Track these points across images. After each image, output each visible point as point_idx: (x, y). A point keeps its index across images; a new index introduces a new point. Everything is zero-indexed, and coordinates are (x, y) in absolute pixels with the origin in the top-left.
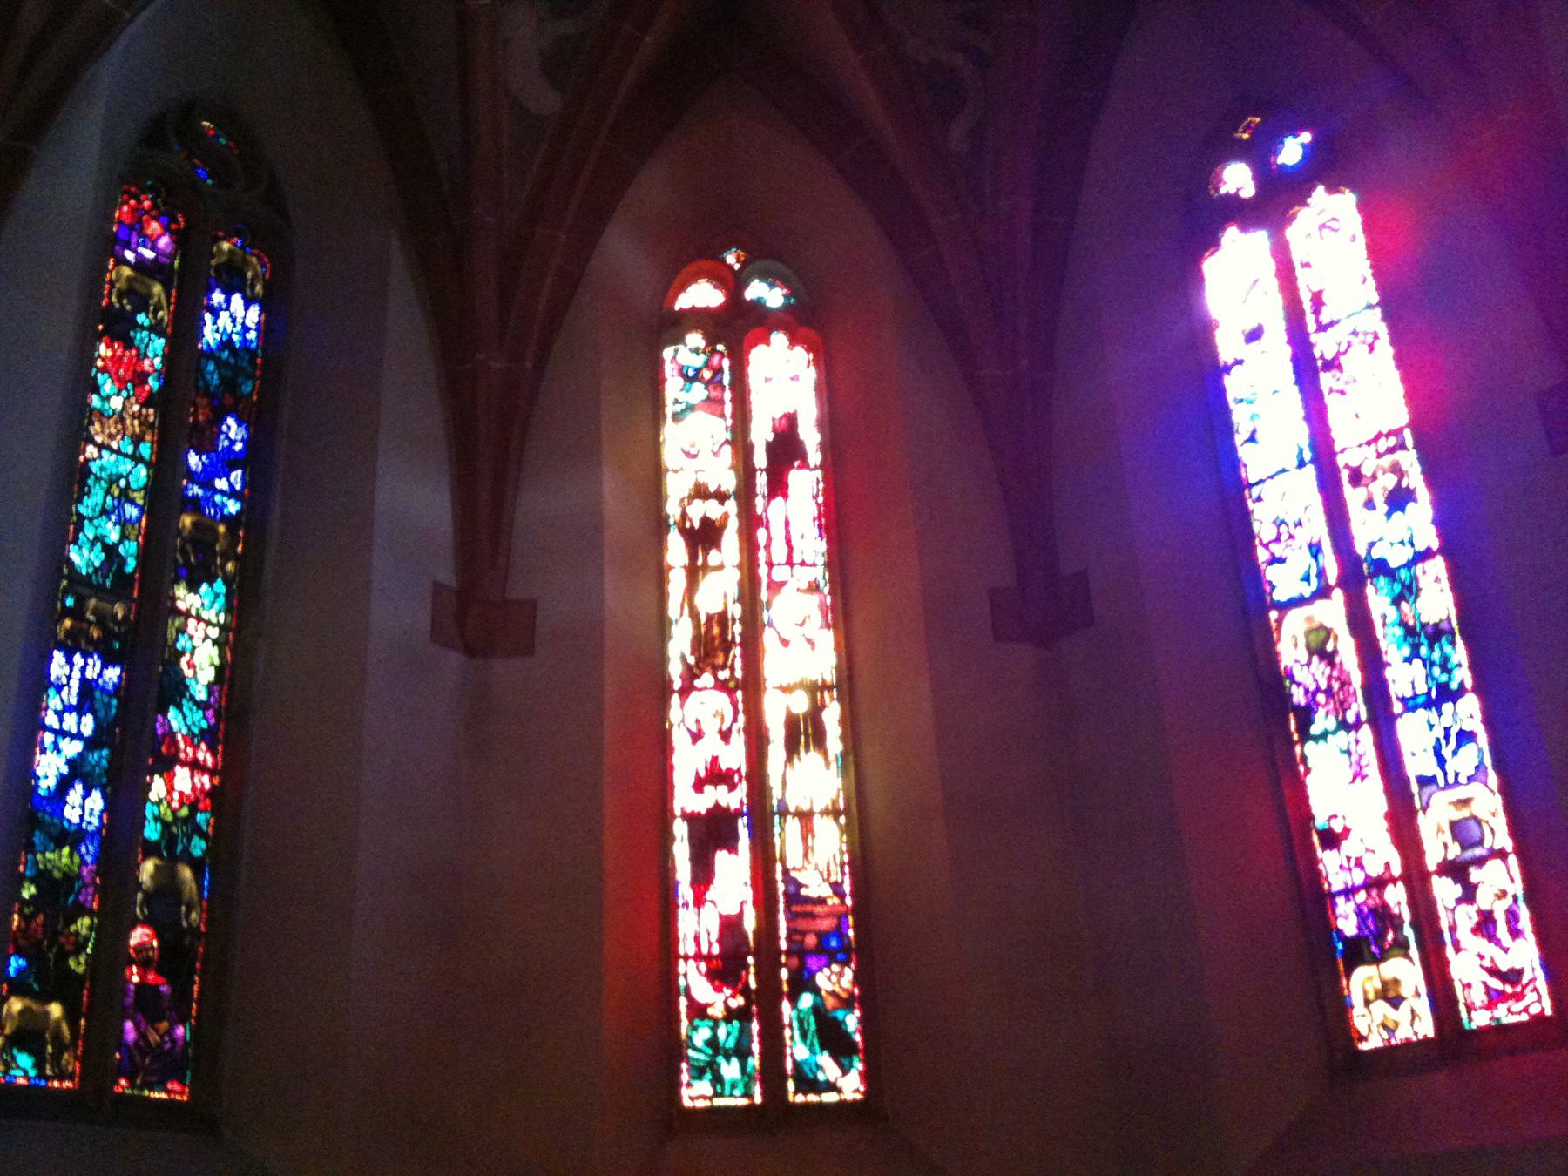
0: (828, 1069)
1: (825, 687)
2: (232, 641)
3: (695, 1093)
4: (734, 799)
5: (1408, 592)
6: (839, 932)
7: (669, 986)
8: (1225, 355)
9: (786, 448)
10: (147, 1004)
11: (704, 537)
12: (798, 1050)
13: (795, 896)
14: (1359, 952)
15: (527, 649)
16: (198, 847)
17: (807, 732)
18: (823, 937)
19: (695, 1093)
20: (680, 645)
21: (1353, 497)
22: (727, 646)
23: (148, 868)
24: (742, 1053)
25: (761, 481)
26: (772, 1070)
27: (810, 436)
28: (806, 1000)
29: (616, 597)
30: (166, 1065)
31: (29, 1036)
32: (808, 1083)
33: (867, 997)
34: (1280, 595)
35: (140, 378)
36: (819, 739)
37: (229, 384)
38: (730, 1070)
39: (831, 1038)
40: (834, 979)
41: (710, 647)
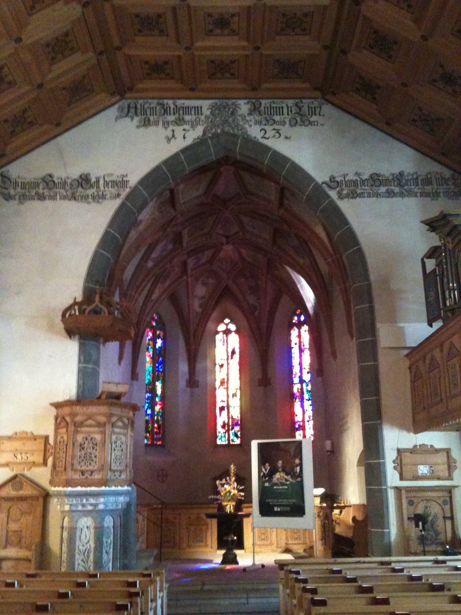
0: (235, 439)
1: (237, 389)
2: (163, 388)
3: (219, 442)
4: (225, 404)
5: (307, 386)
6: (238, 422)
7: (215, 430)
8: (292, 346)
9: (233, 352)
10: (157, 433)
11: (222, 366)
12: (232, 437)
13: (232, 418)
14: (298, 429)
15: (198, 386)
16: (160, 414)
17: (234, 395)
18: (236, 423)
19: (219, 442)
20: (218, 384)
21: (303, 370)
22: (224, 383)
23: (156, 417)
24: (225, 437)
25: (230, 357)
26: (229, 440)
27: (237, 351)
28: (233, 431)
29: (209, 379)
30: (159, 440)
31: (146, 438)
32: (233, 441)
33: (241, 430)
34: (295, 382)
35: (150, 355)
36: (236, 396)
37: (160, 353)
38: (223, 439)
39: (236, 435)
40: (237, 428)
41: (222, 383)
